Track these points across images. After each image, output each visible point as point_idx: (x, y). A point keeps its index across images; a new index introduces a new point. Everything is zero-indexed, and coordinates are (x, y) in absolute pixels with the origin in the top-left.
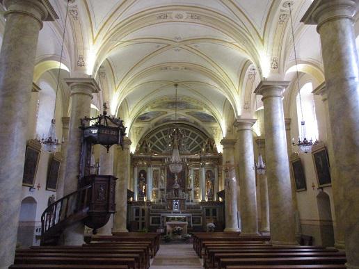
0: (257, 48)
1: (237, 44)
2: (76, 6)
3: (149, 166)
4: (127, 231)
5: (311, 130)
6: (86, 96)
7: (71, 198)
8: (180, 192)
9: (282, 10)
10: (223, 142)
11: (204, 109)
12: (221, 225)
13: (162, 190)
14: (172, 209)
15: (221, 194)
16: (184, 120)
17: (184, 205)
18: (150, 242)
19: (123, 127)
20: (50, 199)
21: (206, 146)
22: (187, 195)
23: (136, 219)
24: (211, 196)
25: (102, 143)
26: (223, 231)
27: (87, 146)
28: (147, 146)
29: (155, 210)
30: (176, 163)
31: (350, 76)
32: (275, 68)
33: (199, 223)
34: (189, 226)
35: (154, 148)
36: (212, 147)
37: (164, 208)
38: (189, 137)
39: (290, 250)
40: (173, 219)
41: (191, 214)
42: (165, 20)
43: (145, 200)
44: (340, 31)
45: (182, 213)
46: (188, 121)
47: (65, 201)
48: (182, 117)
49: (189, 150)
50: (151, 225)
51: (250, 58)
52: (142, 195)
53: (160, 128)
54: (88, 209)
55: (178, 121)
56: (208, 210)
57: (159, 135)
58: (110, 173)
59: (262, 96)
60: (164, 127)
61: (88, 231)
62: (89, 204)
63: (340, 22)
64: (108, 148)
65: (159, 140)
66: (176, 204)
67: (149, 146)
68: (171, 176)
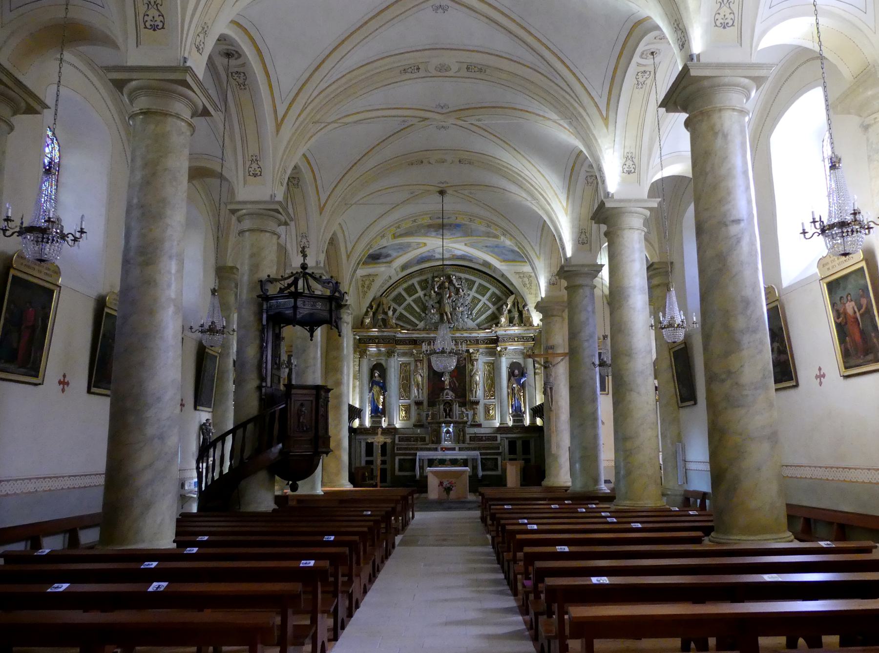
0: (594, 132)
1: (561, 122)
2: (243, 65)
3: (390, 354)
4: (349, 487)
5: (498, 425)
6: (268, 234)
7: (250, 426)
8: (456, 408)
9: (639, 65)
10: (539, 307)
11: (502, 238)
12: (535, 470)
13: (418, 404)
14: (438, 441)
15: (537, 411)
16: (462, 258)
17: (464, 431)
18: (392, 505)
19: (340, 292)
20: (204, 429)
21: (510, 311)
22: (470, 413)
23: (368, 462)
24: (518, 414)
25: (302, 323)
26: (540, 485)
27: (274, 330)
28: (386, 313)
29: (404, 444)
30: (443, 352)
31: (732, 218)
32: (629, 172)
33: (495, 467)
34: (473, 478)
35: (401, 317)
36: (521, 313)
37: (423, 439)
38: (473, 293)
39: (626, 514)
40: (442, 462)
41: (478, 453)
42: (415, 76)
43: (384, 425)
44: (720, 135)
45: (460, 449)
46: (471, 261)
47: (240, 432)
48: (459, 253)
49: (473, 320)
50: (397, 473)
51: (659, 19)
52: (377, 413)
53: (411, 275)
54: (280, 445)
55: (449, 259)
56: (512, 444)
57: (411, 290)
58: (319, 382)
59: (685, 116)
60: (421, 272)
61: (281, 488)
62: (283, 437)
63: (720, 117)
64: (312, 332)
65: (409, 300)
66: (448, 432)
67: (390, 313)
68: (435, 377)
